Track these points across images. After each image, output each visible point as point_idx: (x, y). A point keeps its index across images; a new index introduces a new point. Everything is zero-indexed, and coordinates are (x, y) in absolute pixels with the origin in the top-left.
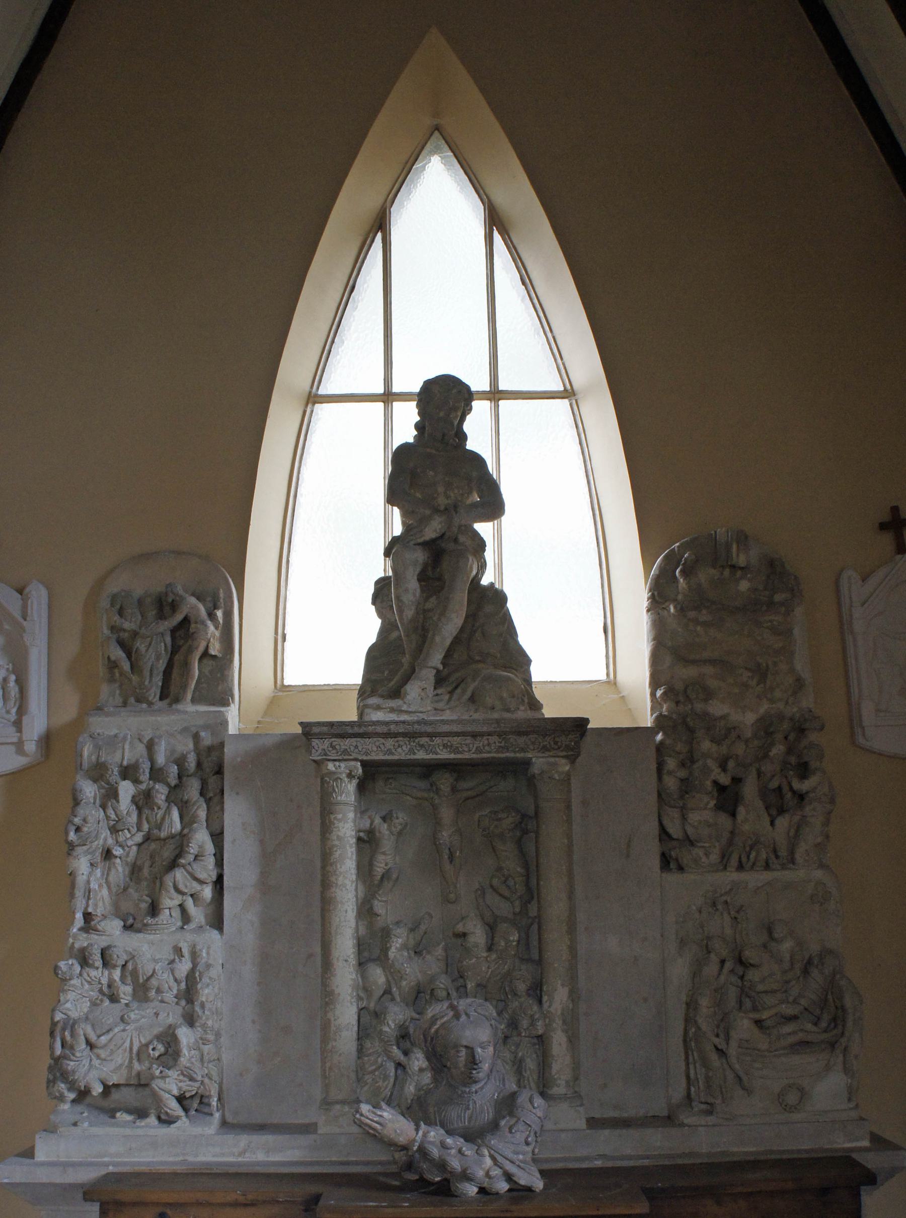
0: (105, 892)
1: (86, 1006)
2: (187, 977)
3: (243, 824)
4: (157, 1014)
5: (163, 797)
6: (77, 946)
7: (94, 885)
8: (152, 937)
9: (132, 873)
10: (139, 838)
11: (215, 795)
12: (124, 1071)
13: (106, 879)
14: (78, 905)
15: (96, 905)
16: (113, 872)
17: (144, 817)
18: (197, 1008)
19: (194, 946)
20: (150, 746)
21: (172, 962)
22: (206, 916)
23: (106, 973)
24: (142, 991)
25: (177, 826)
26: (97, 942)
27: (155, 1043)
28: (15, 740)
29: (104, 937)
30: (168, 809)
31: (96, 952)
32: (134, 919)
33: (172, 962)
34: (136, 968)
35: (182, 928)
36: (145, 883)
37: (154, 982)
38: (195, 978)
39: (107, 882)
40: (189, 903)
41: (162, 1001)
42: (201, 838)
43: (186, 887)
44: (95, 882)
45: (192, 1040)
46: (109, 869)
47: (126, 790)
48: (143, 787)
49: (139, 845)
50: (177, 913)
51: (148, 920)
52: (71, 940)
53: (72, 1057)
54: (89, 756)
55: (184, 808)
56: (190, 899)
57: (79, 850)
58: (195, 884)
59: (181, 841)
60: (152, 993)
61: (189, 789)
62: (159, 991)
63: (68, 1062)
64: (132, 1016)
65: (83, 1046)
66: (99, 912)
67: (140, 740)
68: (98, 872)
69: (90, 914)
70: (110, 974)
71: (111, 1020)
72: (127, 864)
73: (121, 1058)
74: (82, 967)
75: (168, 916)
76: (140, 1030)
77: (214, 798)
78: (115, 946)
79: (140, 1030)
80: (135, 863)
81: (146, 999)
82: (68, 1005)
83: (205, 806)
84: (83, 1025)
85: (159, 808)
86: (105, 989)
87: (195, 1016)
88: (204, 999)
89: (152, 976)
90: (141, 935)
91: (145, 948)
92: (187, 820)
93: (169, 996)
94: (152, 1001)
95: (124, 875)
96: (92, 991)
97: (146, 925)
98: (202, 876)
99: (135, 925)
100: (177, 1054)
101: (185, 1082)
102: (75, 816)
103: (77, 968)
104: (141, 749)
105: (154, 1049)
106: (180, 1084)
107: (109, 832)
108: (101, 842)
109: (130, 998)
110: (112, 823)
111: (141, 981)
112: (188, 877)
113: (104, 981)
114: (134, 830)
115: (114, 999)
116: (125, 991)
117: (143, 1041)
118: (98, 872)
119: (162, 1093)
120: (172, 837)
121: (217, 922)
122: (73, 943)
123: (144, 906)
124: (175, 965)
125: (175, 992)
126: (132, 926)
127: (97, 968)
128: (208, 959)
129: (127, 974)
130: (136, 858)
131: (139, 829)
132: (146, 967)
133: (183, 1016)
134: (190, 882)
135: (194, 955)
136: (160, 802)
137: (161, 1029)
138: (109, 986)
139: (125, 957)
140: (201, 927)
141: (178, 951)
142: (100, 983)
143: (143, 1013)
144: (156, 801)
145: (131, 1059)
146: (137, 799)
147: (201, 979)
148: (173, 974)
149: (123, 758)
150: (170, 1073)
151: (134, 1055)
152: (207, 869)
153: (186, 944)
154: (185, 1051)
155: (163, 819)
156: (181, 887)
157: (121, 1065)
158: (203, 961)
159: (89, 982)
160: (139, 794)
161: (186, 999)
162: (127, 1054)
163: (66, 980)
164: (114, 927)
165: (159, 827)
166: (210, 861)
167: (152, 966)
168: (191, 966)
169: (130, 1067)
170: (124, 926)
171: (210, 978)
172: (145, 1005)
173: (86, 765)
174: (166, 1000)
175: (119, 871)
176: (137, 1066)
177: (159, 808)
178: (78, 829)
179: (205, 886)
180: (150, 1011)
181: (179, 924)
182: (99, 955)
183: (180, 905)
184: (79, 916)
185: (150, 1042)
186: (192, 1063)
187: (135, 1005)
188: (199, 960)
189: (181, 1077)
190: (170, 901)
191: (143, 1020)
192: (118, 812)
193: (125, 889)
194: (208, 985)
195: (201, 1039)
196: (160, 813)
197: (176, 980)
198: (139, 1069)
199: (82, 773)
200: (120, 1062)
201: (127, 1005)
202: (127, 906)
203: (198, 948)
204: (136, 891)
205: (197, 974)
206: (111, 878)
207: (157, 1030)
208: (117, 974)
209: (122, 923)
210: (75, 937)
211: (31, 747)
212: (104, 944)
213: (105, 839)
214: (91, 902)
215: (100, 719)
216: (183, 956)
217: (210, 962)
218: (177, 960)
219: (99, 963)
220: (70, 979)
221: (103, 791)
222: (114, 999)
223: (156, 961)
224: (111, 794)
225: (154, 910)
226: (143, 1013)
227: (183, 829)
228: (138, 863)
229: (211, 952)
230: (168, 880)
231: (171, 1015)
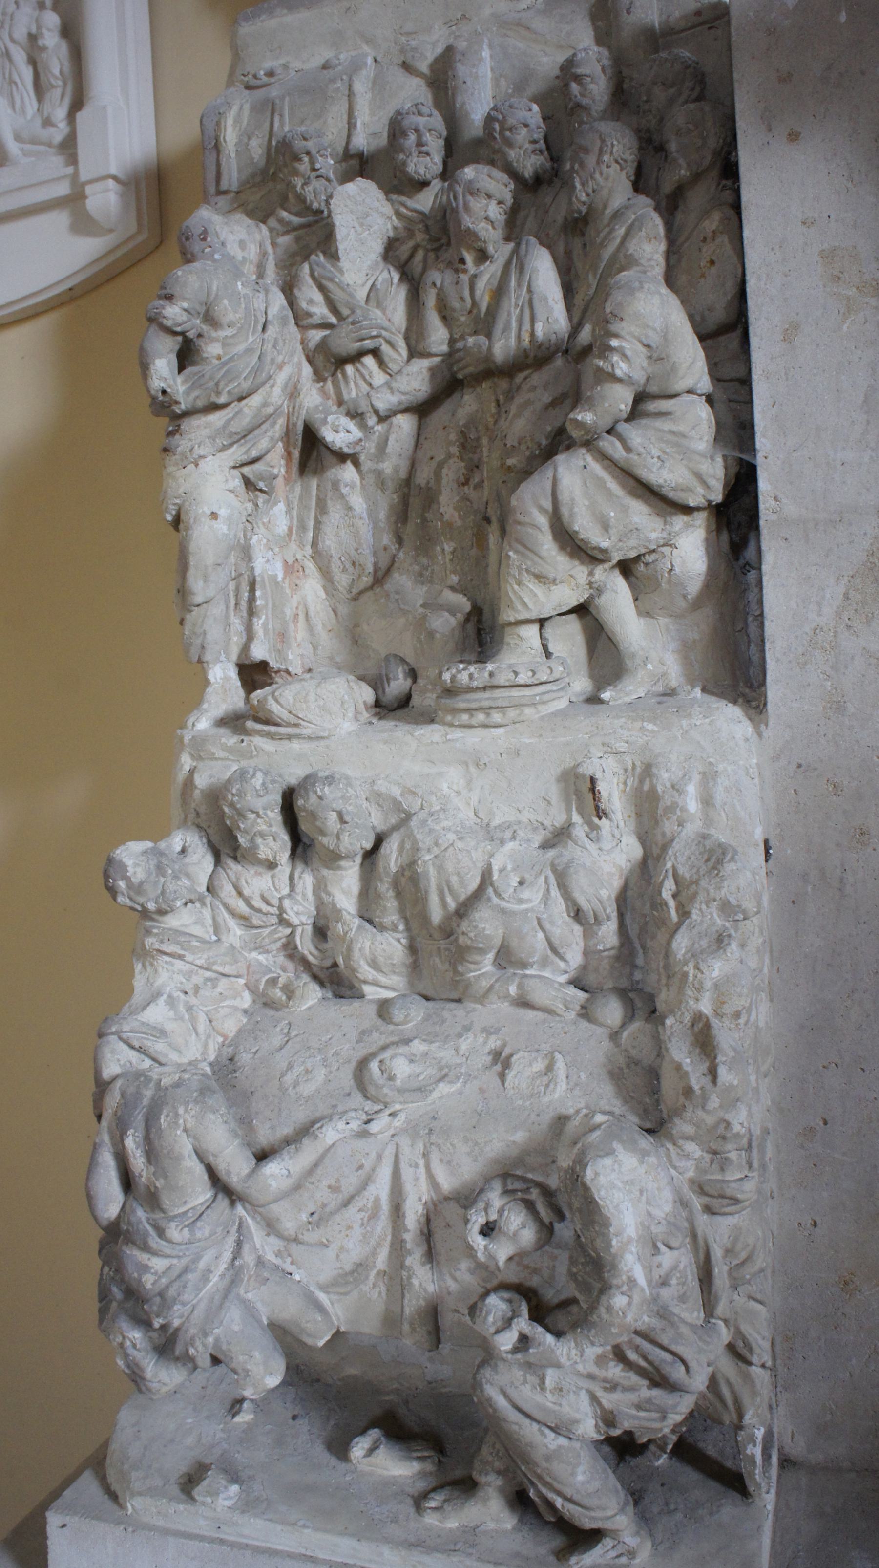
0: (312, 589)
1: (232, 1007)
2: (622, 900)
3: (828, 256)
4: (501, 1061)
5: (495, 211)
6: (201, 781)
7: (267, 564)
8: (473, 739)
9: (401, 514)
10: (416, 380)
11: (697, 177)
12: (374, 1292)
13: (314, 544)
14: (214, 633)
15: (282, 636)
16: (335, 515)
17: (430, 299)
18: (680, 1051)
19: (648, 771)
20: (442, 80)
21: (559, 836)
22: (685, 650)
23: (306, 880)
24: (441, 952)
25: (553, 317)
26: (276, 761)
27: (495, 1198)
28: (63, 189)
29: (296, 745)
30: (517, 262)
31: (258, 804)
32: (413, 674)
33: (559, 836)
34: (413, 863)
35: (594, 700)
36: (448, 547)
37: (486, 924)
38: (659, 905)
39: (318, 555)
40: (618, 601)
41: (523, 1003)
42: (654, 323)
43: (606, 527)
44: (263, 550)
45: (665, 1205)
46: (322, 507)
47: (363, 218)
48: (425, 201)
49: (422, 410)
50: (569, 639)
51: (465, 674)
52: (186, 762)
53: (154, 1241)
54: (243, 148)
55: (579, 244)
56: (619, 583)
57: (199, 431)
58: (640, 513)
59: (572, 362)
60: (483, 969)
61: (591, 160)
62: (506, 958)
63: (143, 1257)
64: (402, 1068)
65: (201, 1194)
66: (294, 661)
67: (406, 67)
68: (279, 516)
69: (263, 666)
70: (320, 887)
71: (320, 1075)
72: (381, 482)
73: (357, 1239)
74: (218, 861)
75: (539, 658)
76: (430, 1131)
77: (698, 188)
78: (330, 780)
79: (430, 1131)
80: (408, 482)
81: (458, 993)
82: (157, 1013)
83: (656, 224)
84: (187, 1115)
85: (483, 256)
86: (306, 945)
87: (669, 1085)
88: (706, 1007)
89: (478, 894)
90: (431, 733)
91: (451, 779)
92: (588, 289)
93: (551, 982)
94: (482, 999)
95: (376, 529)
96: (261, 949)
97: (451, 691)
98: (667, 475)
99: (415, 700)
100: (594, 1270)
101: (632, 1389)
102: (169, 298)
103: (201, 863)
104: (413, 91)
105: (488, 1230)
106: (608, 1400)
107: (307, 370)
108: (276, 394)
109: (398, 981)
110: (316, 336)
111: (436, 915)
112: (612, 485)
113: (301, 913)
114: (396, 355)
115: (337, 982)
116: (379, 955)
117: (447, 1183)
118: (279, 516)
119: (529, 1431)
120: (536, 357)
121: (735, 666)
122: (192, 772)
123: (444, 624)
124: (568, 852)
125: (575, 958)
126: (404, 702)
127: (271, 865)
128: (708, 821)
129: (384, 888)
130: (413, 465)
131: (414, 353)
132: (453, 861)
133: (616, 1076)
134: (611, 509)
135: (649, 807)
136: (484, 230)
137: (519, 1136)
138: (321, 932)
139: (378, 820)
140: (671, 693)
141: (584, 792)
142: (283, 921)
143: (446, 1055)
144: (467, 222)
145: (398, 1248)
146: (404, 250)
147: (684, 914)
148: (563, 887)
149: (351, 125)
150: (563, 1350)
151: (410, 1237)
152: (684, 452)
153: (611, 764)
154: (632, 1265)
155: (499, 292)
156: (585, 527)
157: (361, 1267)
158: (691, 829)
159: (244, 920)
160: (410, 233)
161: (623, 994)
162: (383, 1225)
163: (145, 914)
164: (327, 710)
165: (485, 324)
166: (697, 421)
167: (479, 857)
168: (637, 852)
169: (396, 1278)
170: (378, 704)
171: (726, 908)
172: (454, 1014)
173: (232, 176)
174: (540, 995)
175: (357, 507)
176: (424, 1281)
177: (483, 256)
178: (187, 355)
179: (679, 521)
180: (474, 1047)
181: (582, 684)
182: (275, 816)
183: (582, 610)
184: (223, 674)
185: (466, 1198)
186: (663, 1314)
187: (415, 1013)
188: (669, 826)
189: (615, 1371)
190: (541, 587)
191: (444, 1088)
192: (338, 294)
193: (380, 577)
194: (720, 941)
195: (700, 1188)
196: (489, 274)
197: (578, 914)
198: (431, 1288)
199: (222, 201)
200: (355, 1252)
201: (384, 1009)
202: (386, 635)
203: (664, 778)
204: (421, 578)
205: (668, 889)
206: (329, 542)
207: (503, 1140)
208: (345, 887)
209: (367, 694)
210: (199, 748)
211: (104, 200)
212: (294, 775)
213: (293, 393)
214: (258, 624)
215: (272, 23)
216: (600, 813)
217: (720, 835)
218: (580, 831)
219: (275, 843)
220: (162, 912)
221: (285, 240)
222: (337, 982)
223: (493, 834)
224: (315, 236)
225: (481, 634)
226: (446, 1055)
227: (576, 329)
228: (423, 476)
229: (720, 795)
230: (531, 503)
231: (563, 1070)
